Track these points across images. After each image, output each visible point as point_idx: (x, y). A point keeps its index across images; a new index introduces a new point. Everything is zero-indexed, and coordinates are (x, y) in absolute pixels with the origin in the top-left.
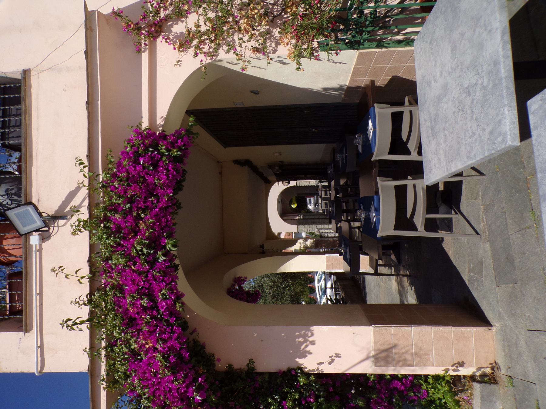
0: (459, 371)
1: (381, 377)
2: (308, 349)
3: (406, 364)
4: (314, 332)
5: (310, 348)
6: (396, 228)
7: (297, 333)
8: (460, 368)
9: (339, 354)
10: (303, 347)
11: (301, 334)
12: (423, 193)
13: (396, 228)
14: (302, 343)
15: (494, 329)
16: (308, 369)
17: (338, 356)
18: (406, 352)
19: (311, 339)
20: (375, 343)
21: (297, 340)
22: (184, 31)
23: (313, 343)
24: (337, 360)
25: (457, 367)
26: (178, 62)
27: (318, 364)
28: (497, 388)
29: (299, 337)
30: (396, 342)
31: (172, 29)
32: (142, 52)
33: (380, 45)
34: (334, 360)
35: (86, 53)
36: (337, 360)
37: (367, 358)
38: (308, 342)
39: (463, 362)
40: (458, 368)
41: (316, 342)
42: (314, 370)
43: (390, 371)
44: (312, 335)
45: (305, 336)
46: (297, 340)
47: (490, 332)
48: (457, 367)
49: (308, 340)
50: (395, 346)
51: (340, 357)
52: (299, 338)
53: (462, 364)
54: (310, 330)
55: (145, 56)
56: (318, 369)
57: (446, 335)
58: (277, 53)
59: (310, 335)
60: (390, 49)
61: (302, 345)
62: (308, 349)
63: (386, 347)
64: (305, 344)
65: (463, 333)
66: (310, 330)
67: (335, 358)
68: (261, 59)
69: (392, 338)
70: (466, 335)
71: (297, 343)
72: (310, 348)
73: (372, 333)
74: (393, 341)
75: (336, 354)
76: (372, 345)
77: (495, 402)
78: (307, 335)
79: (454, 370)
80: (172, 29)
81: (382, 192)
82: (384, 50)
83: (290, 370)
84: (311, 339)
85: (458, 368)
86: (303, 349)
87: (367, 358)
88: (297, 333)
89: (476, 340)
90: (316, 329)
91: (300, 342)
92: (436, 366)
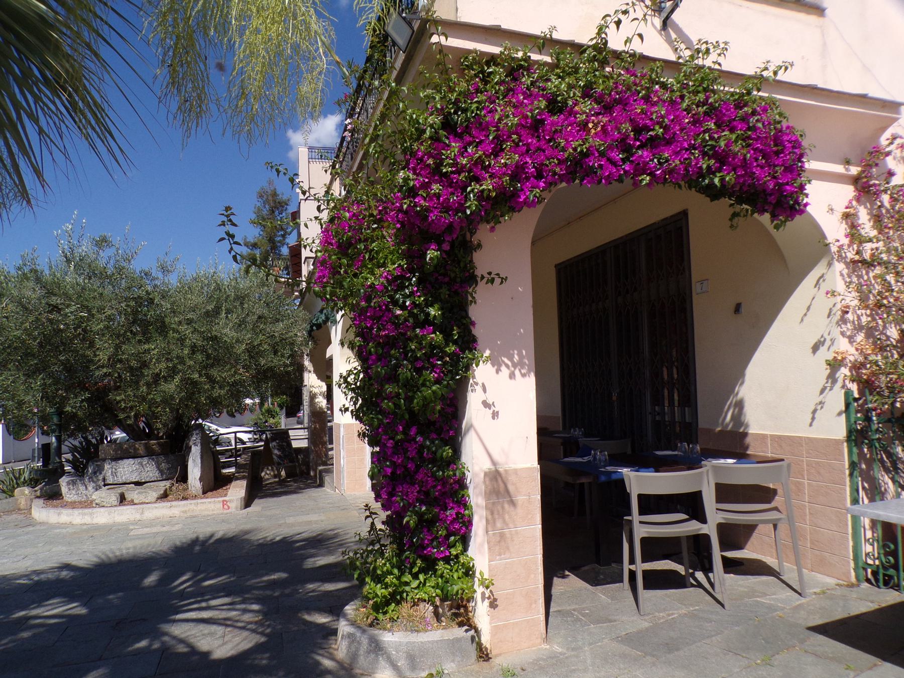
0: (483, 600)
1: (461, 484)
2: (503, 368)
3: (490, 523)
4: (527, 378)
5: (505, 372)
6: (640, 497)
7: (524, 352)
8: (487, 602)
9: (497, 416)
10: (506, 360)
11: (524, 357)
12: (693, 531)
13: (640, 497)
14: (511, 359)
15: (546, 646)
16: (475, 368)
17: (495, 415)
18: (504, 521)
19: (517, 372)
20: (516, 471)
21: (516, 352)
22: (860, 222)
23: (512, 376)
24: (489, 412)
25: (489, 598)
26: (832, 210)
27: (483, 385)
28: (474, 660)
29: (520, 354)
30: (520, 503)
31: (863, 206)
32: (845, 165)
33: (853, 465)
34: (490, 409)
35: (864, 97)
36: (489, 412)
37: (494, 463)
38: (513, 369)
39: (497, 606)
40: (486, 600)
41: (513, 381)
42: (474, 377)
43: (476, 498)
44: (523, 375)
45: (520, 364)
46: (516, 352)
47: (539, 640)
48: (489, 598)
49: (515, 369)
50: (513, 503)
51: (493, 418)
52: (518, 354)
53: (493, 605)
54: (529, 372)
55: (839, 169)
56: (477, 384)
57: (532, 576)
58: (841, 336)
59: (523, 371)
60: (848, 479)
61: (509, 359)
62: (503, 368)
63: (511, 488)
64: (509, 363)
65: (536, 602)
66: (529, 372)
67: (492, 410)
68: (829, 316)
69: (524, 495)
70: (534, 606)
71: (511, 352)
72: (505, 372)
73: (529, 465)
74: (520, 498)
75: (498, 412)
76: (513, 466)
77: (453, 661)
78: (522, 367)
79: (483, 594)
80: (863, 206)
81: (695, 474)
82: (847, 472)
83: (474, 340)
84: (517, 372)
85: (486, 600)
86: (503, 362)
87: (494, 463)
88: (524, 352)
89: (528, 621)
90: (531, 380)
91: (513, 355)
92: (490, 566)
